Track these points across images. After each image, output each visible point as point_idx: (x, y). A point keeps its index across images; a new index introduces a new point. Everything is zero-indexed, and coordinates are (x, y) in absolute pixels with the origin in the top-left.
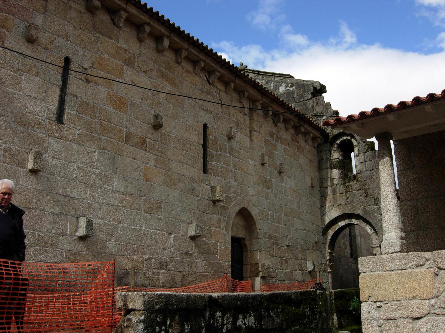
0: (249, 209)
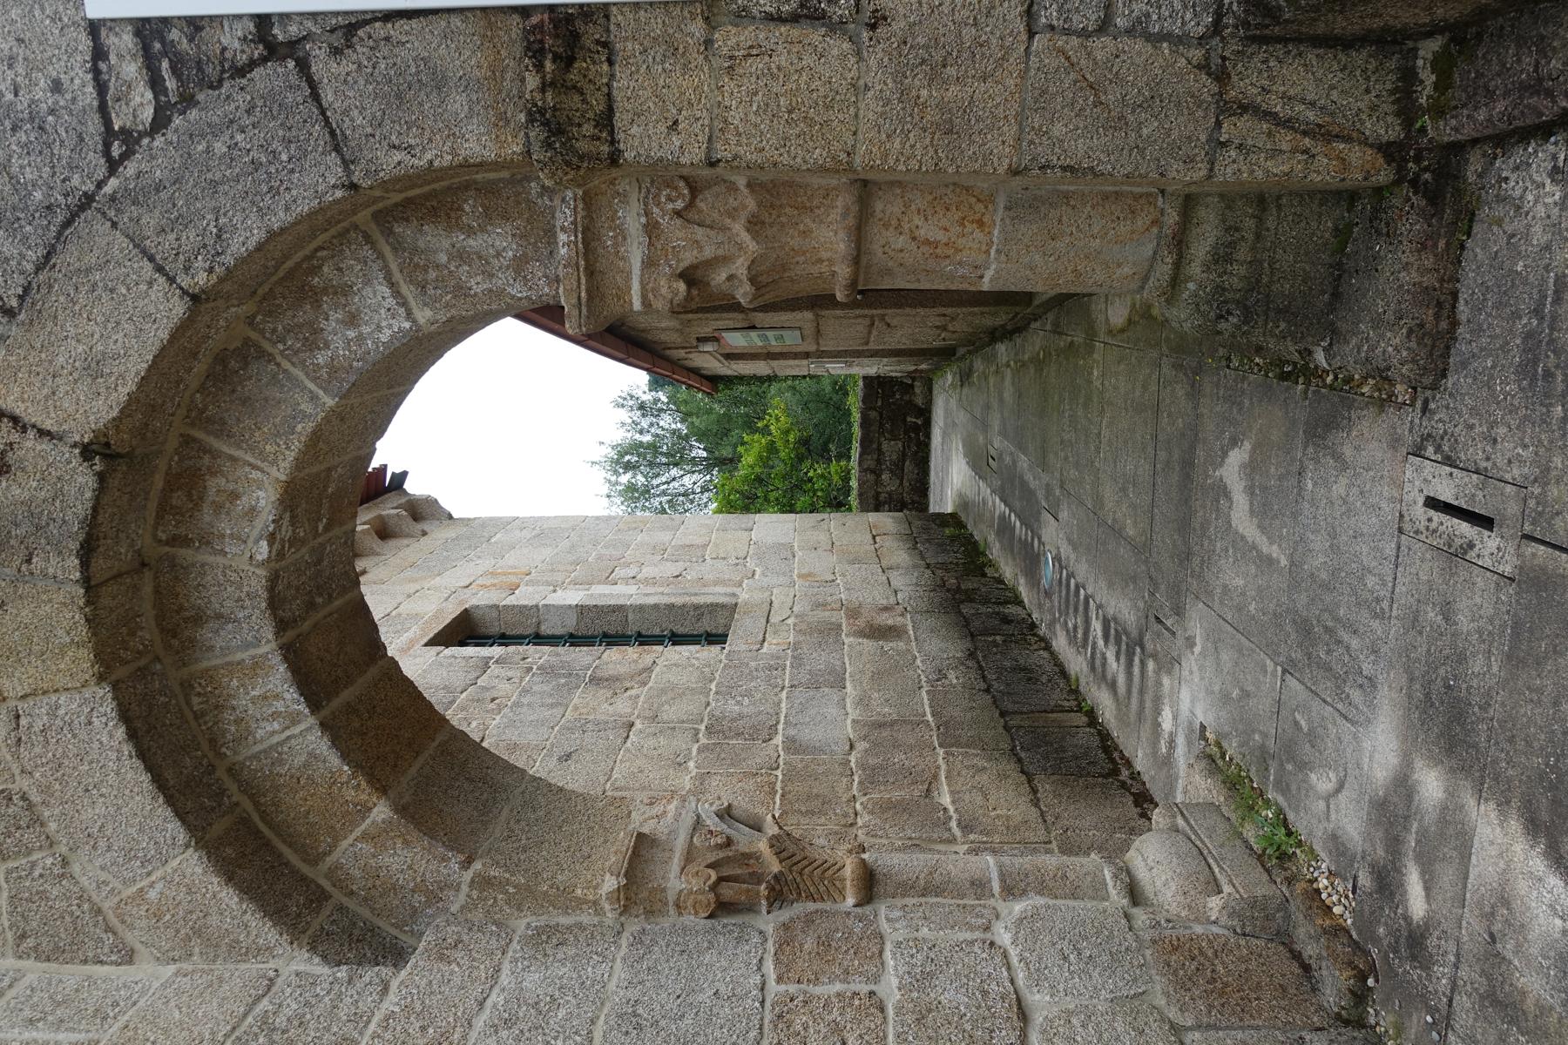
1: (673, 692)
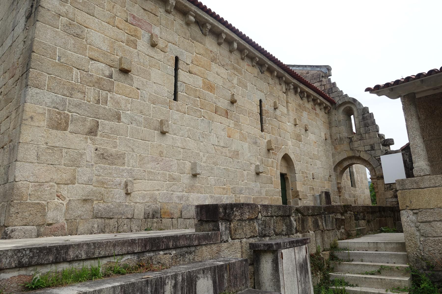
1: (347, 183)
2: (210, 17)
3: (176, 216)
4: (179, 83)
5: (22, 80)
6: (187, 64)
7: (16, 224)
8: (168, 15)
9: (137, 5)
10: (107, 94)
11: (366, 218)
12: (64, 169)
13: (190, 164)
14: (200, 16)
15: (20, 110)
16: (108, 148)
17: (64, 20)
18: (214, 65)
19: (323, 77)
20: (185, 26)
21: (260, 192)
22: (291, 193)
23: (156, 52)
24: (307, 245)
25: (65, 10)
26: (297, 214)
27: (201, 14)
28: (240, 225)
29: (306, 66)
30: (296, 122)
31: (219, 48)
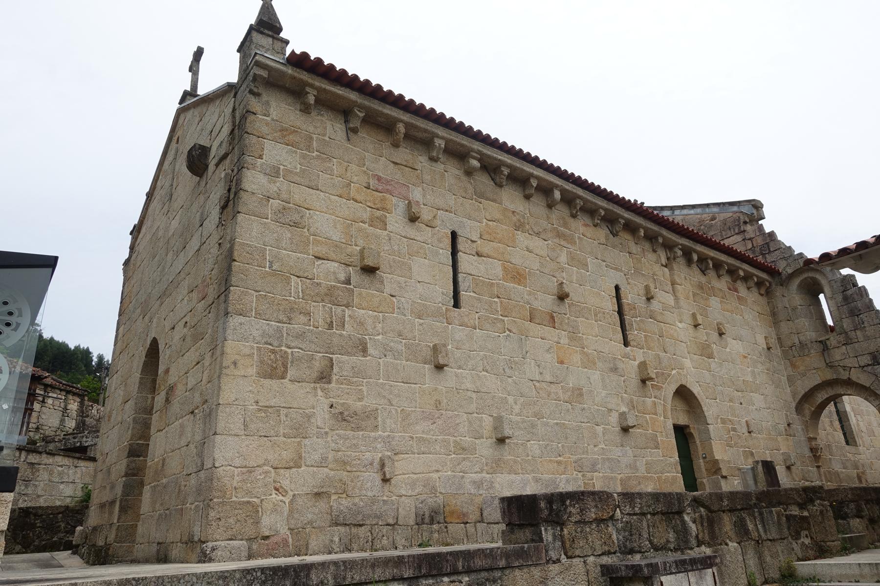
0: (688, 386)
2: (506, 155)
3: (473, 517)
4: (461, 277)
5: (219, 304)
6: (472, 241)
7: (218, 537)
8: (434, 164)
9: (383, 159)
10: (344, 311)
11: (866, 513)
12: (284, 443)
13: (491, 419)
14: (489, 157)
15: (218, 352)
16: (350, 402)
17: (275, 203)
18: (520, 236)
19: (745, 223)
20: (464, 178)
21: (633, 467)
22: (702, 464)
23: (418, 230)
24: (715, 569)
25: (276, 189)
26: (697, 507)
27: (489, 153)
28: (581, 532)
29: (708, 205)
30: (696, 319)
31: (527, 205)
